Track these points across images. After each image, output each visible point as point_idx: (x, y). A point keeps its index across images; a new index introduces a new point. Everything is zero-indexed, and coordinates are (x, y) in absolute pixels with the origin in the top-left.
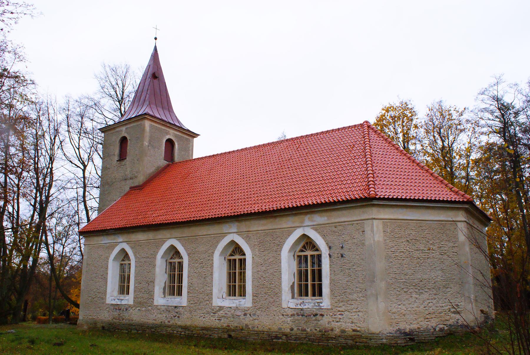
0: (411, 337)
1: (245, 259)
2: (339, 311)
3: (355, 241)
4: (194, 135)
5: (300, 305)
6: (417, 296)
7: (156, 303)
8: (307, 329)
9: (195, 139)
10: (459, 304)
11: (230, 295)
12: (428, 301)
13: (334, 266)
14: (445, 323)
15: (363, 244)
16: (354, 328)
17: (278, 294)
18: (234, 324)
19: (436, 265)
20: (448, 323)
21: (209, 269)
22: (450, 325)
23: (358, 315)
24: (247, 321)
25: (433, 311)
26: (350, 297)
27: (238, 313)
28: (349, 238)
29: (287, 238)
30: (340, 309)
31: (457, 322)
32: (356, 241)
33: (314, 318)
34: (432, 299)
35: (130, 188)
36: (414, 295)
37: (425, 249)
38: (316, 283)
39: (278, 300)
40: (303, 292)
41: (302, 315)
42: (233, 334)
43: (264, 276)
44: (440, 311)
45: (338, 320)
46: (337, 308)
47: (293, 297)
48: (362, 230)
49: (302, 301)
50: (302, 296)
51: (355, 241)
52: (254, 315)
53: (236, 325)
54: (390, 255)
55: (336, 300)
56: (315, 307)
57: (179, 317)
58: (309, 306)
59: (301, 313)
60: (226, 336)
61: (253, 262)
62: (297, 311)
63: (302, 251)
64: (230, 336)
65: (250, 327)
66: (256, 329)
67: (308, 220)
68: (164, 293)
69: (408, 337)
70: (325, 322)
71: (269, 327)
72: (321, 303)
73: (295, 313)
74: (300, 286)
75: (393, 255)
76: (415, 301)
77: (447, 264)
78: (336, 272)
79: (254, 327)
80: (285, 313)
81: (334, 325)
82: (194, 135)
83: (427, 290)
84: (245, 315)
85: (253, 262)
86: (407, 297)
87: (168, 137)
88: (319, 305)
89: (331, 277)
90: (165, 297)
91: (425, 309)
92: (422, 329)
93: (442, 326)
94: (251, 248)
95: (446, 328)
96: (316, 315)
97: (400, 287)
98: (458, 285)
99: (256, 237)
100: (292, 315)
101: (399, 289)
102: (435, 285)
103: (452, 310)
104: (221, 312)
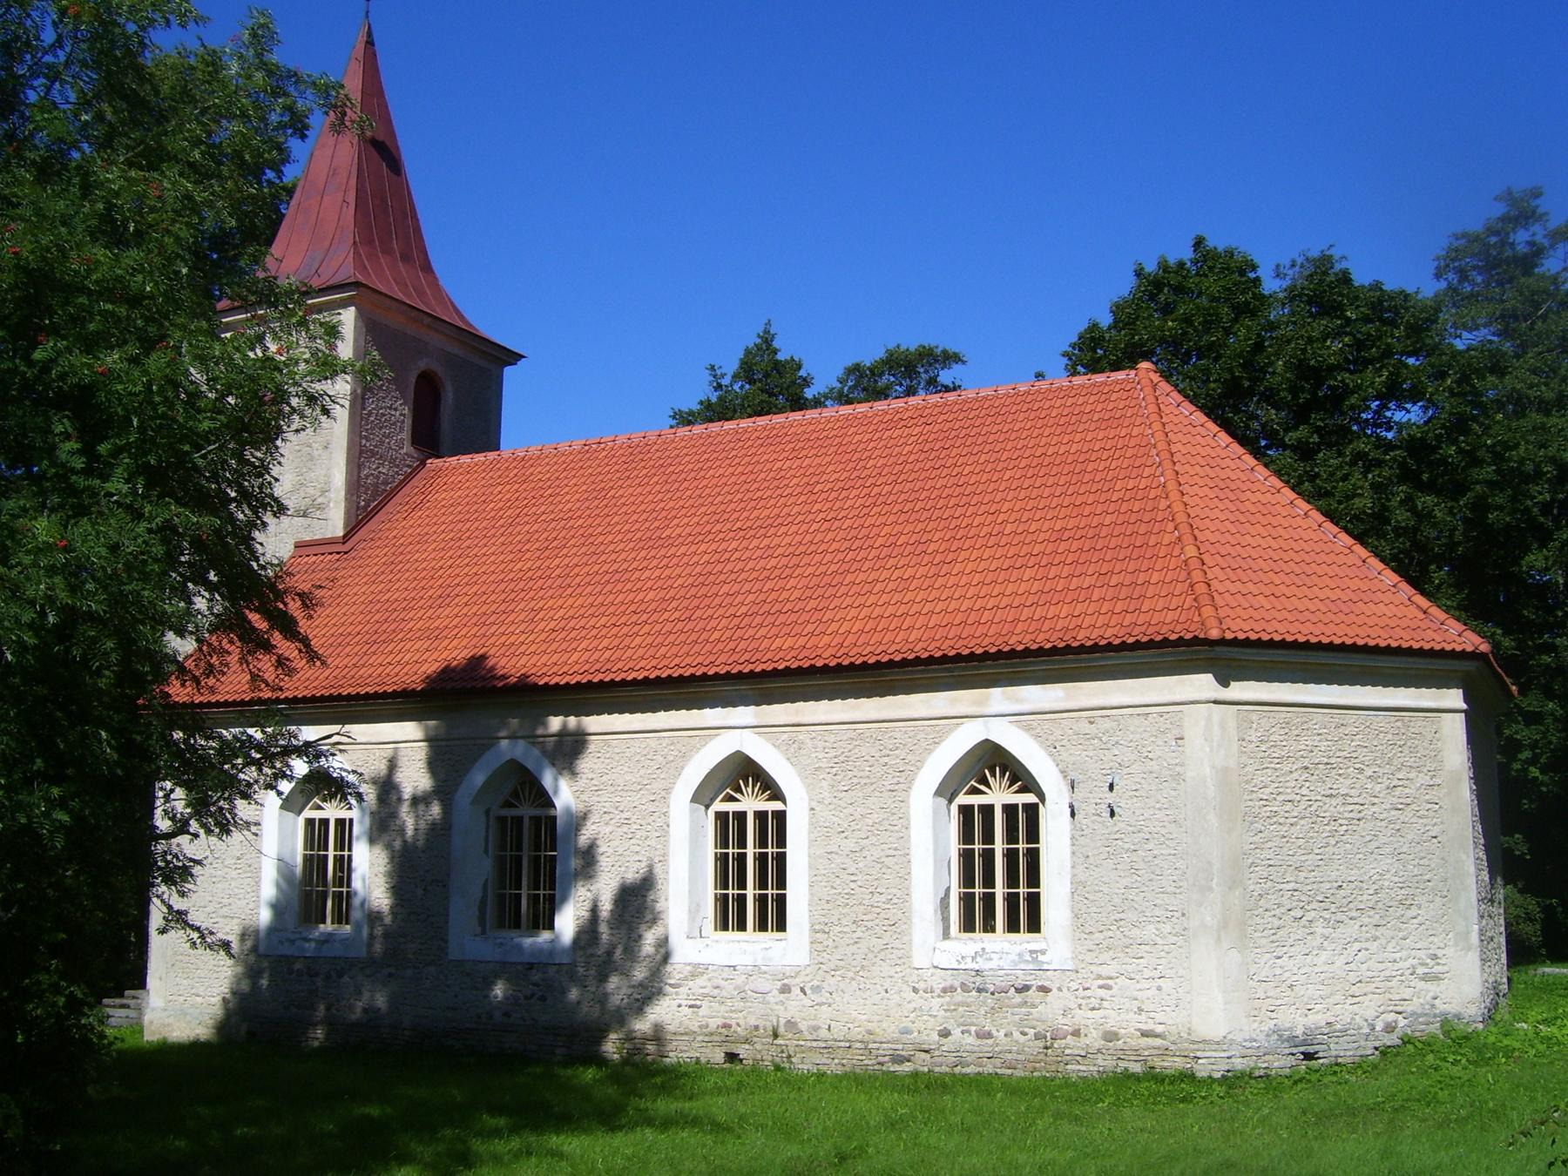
0: (1311, 1049)
1: (780, 817)
2: (1099, 977)
3: (1154, 766)
4: (514, 357)
5: (973, 958)
6: (1327, 932)
7: (454, 953)
8: (994, 1033)
9: (508, 371)
10: (1440, 953)
11: (725, 927)
12: (1357, 946)
13: (1082, 841)
14: (1399, 1009)
15: (1178, 777)
16: (1144, 1027)
17: (897, 925)
18: (745, 1018)
19: (1382, 840)
20: (1409, 1008)
21: (653, 843)
22: (1413, 1014)
23: (1159, 989)
24: (794, 1008)
25: (1370, 974)
26: (1135, 932)
27: (762, 984)
28: (1133, 757)
29: (930, 752)
30: (1104, 971)
31: (1433, 1006)
32: (1156, 768)
33: (1018, 998)
34: (1367, 940)
35: (298, 546)
36: (1319, 928)
37: (1353, 792)
38: (770, 850)
39: (897, 944)
40: (976, 916)
41: (979, 991)
42: (743, 1051)
43: (852, 870)
44: (1387, 973)
45: (1094, 1002)
46: (1092, 968)
47: (946, 934)
48: (1176, 732)
49: (978, 947)
50: (973, 930)
51: (1154, 766)
52: (816, 989)
53: (752, 1021)
54: (1257, 810)
55: (1090, 944)
56: (1023, 966)
57: (543, 999)
58: (1002, 963)
59: (976, 984)
60: (718, 1056)
61: (811, 824)
62: (962, 977)
63: (508, 804)
64: (732, 1057)
65: (803, 1026)
66: (823, 1033)
67: (998, 698)
68: (482, 920)
69: (1302, 1049)
70: (1051, 1011)
71: (870, 1026)
72: (1043, 952)
73: (957, 984)
74: (967, 901)
75: (1265, 812)
76: (1321, 947)
77: (1410, 837)
78: (1091, 860)
79: (816, 1028)
80: (921, 986)
81: (1081, 1017)
82: (514, 357)
83: (1354, 914)
84: (786, 989)
85: (813, 825)
86: (1301, 933)
87: (422, 364)
88: (1035, 960)
89: (1074, 875)
90: (484, 932)
91: (1347, 967)
92: (1338, 1027)
93: (1391, 1017)
94: (804, 778)
95: (1402, 1022)
96: (1026, 988)
97: (1279, 905)
98: (1438, 899)
99: (821, 744)
100: (944, 990)
101: (1277, 912)
102: (1375, 898)
103: (1421, 970)
104: (701, 981)
